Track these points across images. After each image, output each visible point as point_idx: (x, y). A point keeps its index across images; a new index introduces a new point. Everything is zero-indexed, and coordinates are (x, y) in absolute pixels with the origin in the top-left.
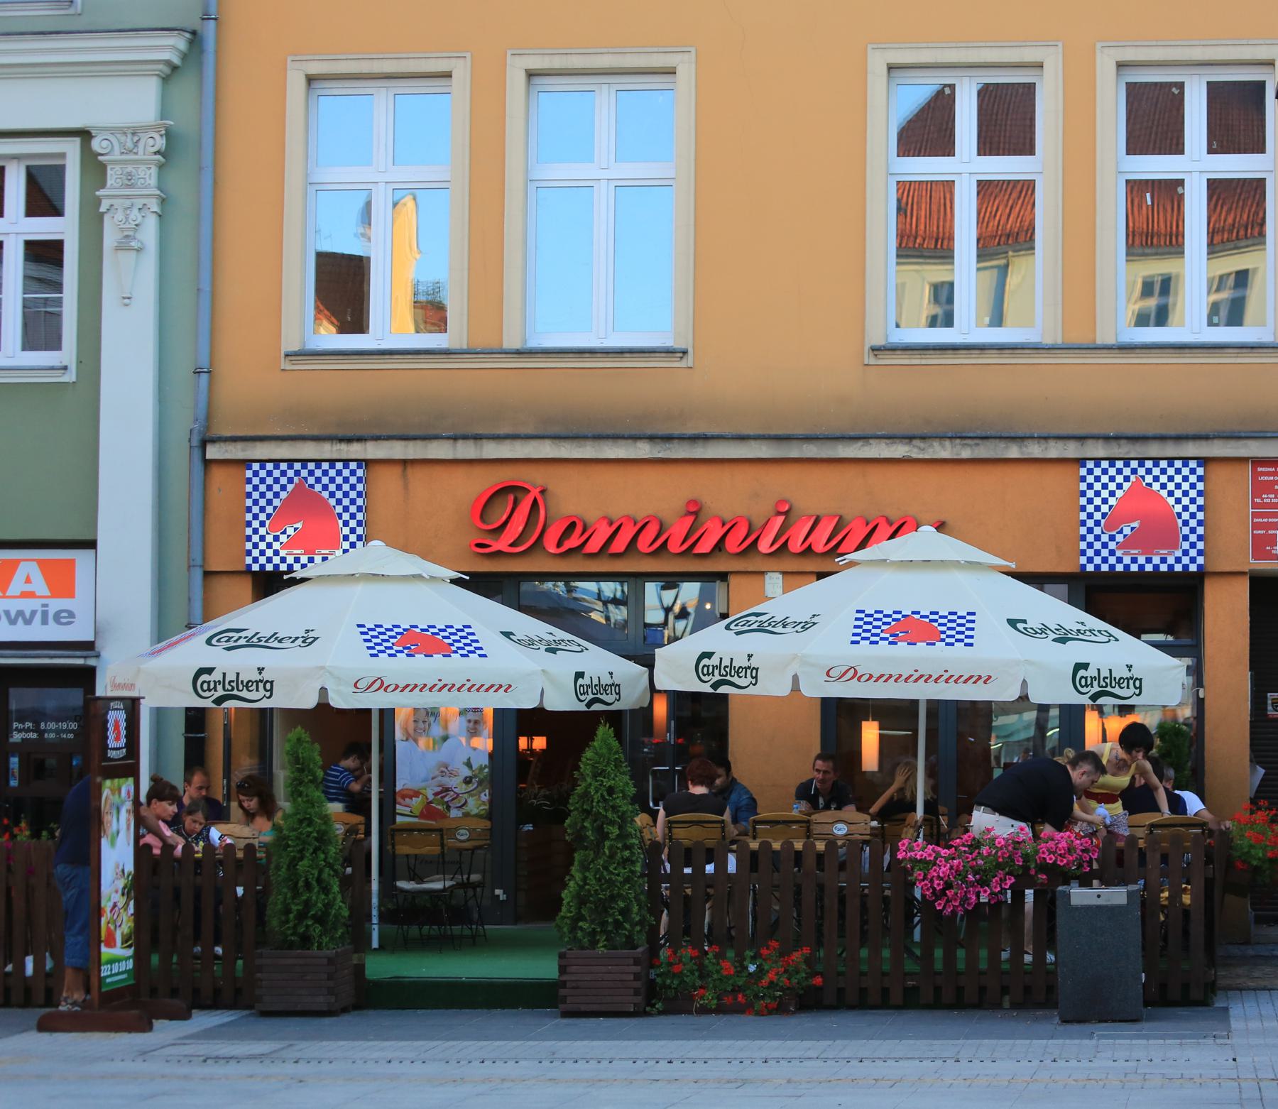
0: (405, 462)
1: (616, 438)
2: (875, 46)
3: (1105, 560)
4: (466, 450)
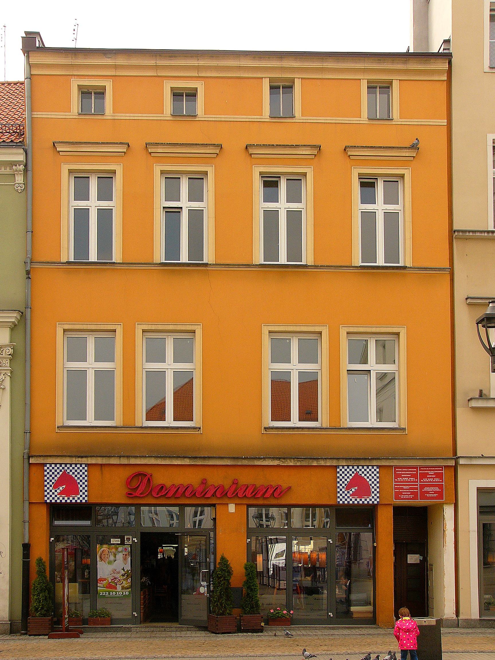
0: (101, 465)
1: (178, 457)
2: (264, 324)
3: (346, 500)
4: (124, 461)
